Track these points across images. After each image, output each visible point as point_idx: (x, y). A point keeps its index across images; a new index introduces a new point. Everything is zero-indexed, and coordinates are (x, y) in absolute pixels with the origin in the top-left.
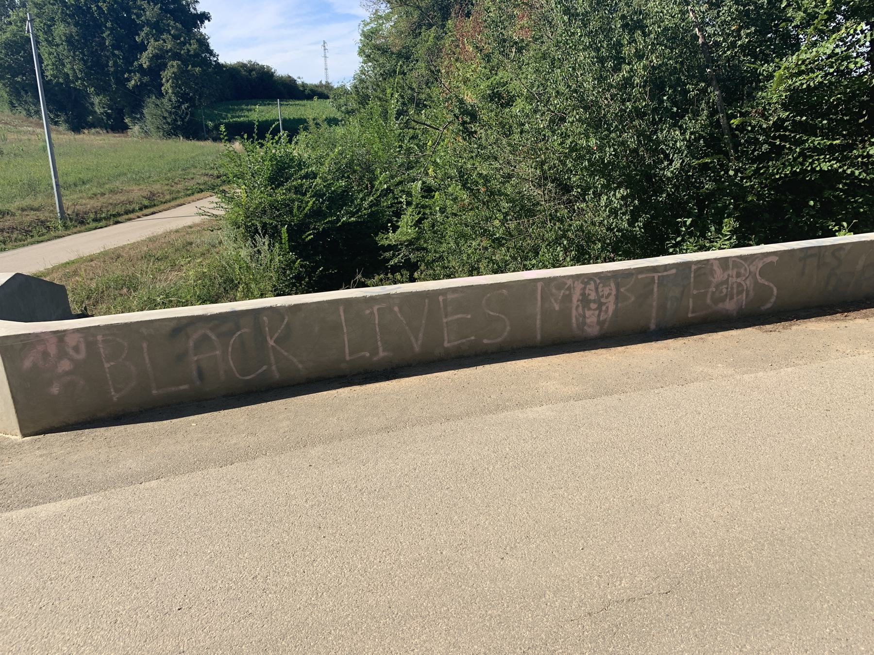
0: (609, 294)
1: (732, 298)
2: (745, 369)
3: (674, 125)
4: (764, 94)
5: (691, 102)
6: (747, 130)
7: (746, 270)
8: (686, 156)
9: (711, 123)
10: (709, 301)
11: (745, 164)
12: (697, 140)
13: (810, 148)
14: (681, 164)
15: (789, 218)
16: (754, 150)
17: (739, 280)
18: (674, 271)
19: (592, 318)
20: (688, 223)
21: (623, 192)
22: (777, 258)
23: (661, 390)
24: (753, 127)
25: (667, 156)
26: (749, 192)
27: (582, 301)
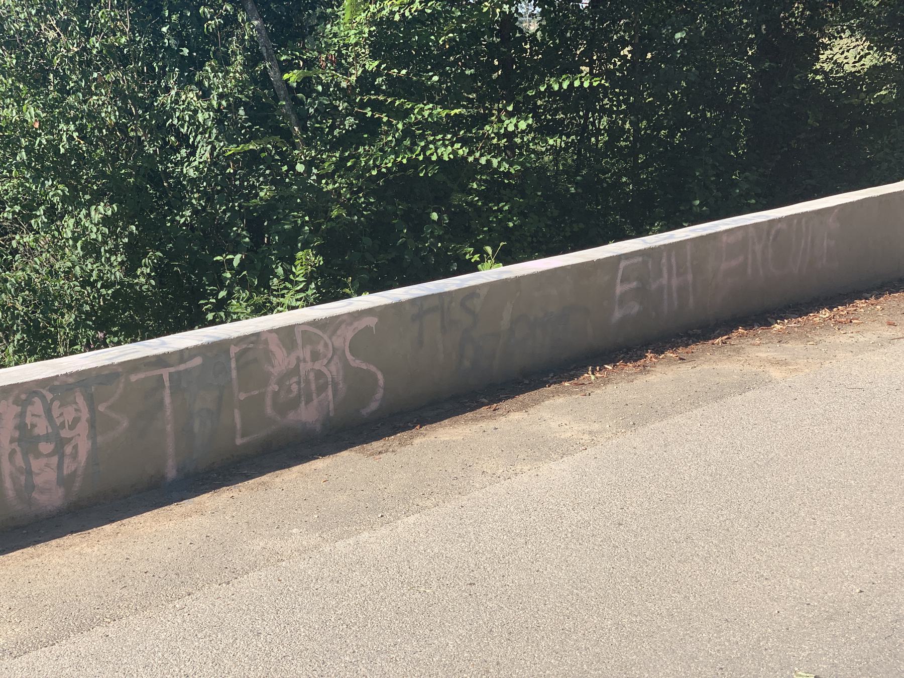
0: (76, 420)
1: (309, 401)
2: (338, 531)
3: (185, 82)
4: (335, 29)
5: (211, 38)
6: (317, 91)
7: (326, 345)
8: (216, 138)
9: (254, 80)
10: (269, 411)
11: (321, 152)
12: (234, 107)
13: (418, 123)
14: (211, 154)
15: (404, 244)
16: (332, 128)
17: (317, 366)
18: (198, 361)
19: (45, 472)
20: (236, 263)
21: (102, 210)
22: (376, 320)
23: (188, 600)
24: (326, 86)
25: (183, 139)
26: (333, 201)
27: (19, 440)
